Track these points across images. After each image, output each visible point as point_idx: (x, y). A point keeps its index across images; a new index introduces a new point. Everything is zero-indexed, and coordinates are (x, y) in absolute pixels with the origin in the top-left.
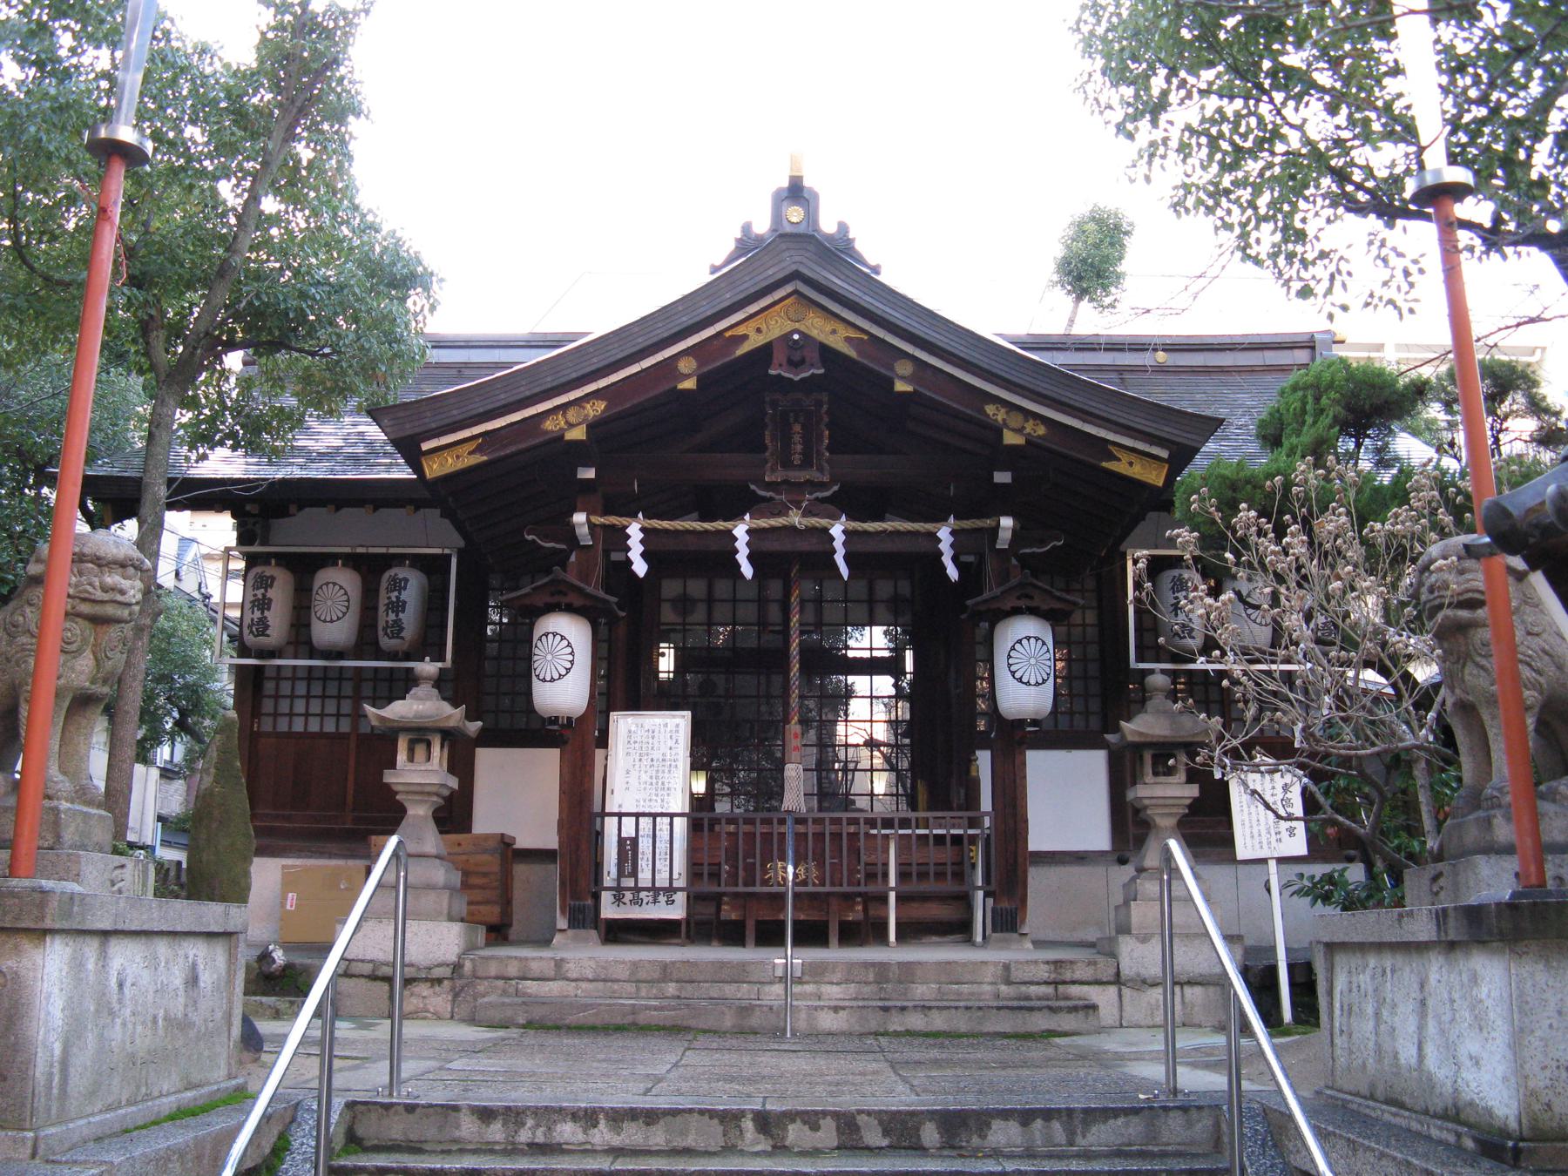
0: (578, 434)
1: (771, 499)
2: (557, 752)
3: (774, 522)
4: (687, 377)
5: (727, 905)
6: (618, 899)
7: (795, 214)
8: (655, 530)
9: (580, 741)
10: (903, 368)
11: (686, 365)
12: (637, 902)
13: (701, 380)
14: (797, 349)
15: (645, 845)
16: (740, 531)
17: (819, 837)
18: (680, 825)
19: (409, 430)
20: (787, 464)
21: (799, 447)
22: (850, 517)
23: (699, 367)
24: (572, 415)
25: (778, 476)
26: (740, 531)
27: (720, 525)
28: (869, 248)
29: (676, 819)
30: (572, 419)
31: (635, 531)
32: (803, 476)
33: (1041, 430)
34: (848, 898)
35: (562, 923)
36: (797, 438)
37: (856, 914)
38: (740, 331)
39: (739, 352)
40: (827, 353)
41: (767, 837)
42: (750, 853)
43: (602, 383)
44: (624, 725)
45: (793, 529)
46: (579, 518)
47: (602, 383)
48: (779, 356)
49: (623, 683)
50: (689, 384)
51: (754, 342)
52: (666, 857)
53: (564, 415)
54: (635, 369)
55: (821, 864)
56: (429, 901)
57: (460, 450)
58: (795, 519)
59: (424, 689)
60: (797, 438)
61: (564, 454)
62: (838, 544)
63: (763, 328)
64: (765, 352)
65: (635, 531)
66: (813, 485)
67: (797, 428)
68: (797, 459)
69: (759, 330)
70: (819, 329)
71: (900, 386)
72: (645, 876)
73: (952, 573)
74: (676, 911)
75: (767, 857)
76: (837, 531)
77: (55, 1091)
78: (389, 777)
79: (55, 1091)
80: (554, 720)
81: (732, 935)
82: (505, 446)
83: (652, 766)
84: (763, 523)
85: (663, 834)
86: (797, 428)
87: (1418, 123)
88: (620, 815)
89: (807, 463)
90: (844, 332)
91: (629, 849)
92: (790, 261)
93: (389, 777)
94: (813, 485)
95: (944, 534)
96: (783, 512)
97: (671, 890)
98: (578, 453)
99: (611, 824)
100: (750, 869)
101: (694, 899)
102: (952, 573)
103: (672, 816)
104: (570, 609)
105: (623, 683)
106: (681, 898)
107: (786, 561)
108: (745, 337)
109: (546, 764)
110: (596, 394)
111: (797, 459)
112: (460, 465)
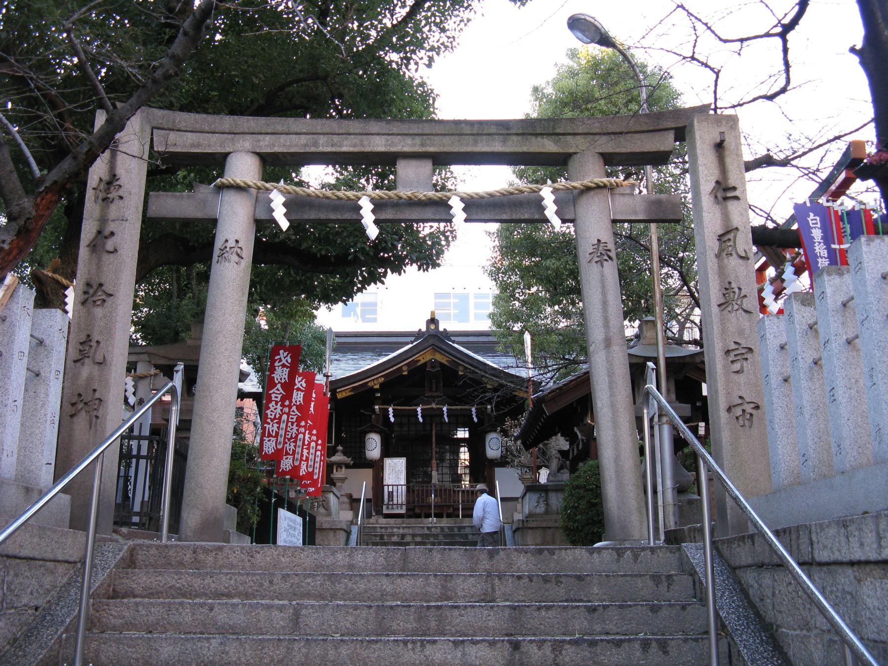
0: (377, 387)
2: (371, 470)
5: (416, 508)
6: (388, 508)
7: (433, 327)
9: (377, 467)
10: (461, 368)
11: (405, 368)
12: (393, 508)
14: (434, 363)
15: (395, 494)
16: (419, 409)
17: (441, 490)
18: (404, 488)
19: (334, 387)
20: (431, 391)
25: (429, 394)
26: (419, 409)
27: (414, 407)
31: (391, 410)
32: (436, 394)
34: (448, 507)
35: (374, 514)
37: (451, 511)
40: (441, 364)
41: (427, 491)
42: (423, 495)
44: (389, 462)
46: (377, 407)
48: (429, 365)
49: (388, 452)
50: (405, 373)
51: (422, 361)
52: (401, 496)
55: (441, 497)
56: (344, 505)
58: (434, 406)
59: (339, 453)
61: (372, 390)
62: (445, 413)
63: (425, 357)
64: (425, 364)
65: (391, 410)
66: (438, 397)
70: (439, 357)
71: (460, 373)
72: (395, 502)
73: (475, 420)
74: (403, 511)
75: (427, 496)
76: (445, 409)
77: (833, 188)
78: (332, 476)
79: (833, 188)
80: (371, 461)
81: (419, 516)
83: (395, 471)
85: (400, 491)
89: (437, 391)
90: (445, 359)
91: (391, 494)
92: (431, 341)
93: (332, 476)
94: (438, 397)
95: (473, 409)
96: (430, 404)
97: (402, 504)
98: (377, 391)
99: (386, 488)
100: (423, 499)
101: (407, 509)
102: (475, 420)
104: (376, 432)
105: (388, 452)
106: (404, 507)
107: (432, 416)
109: (368, 473)
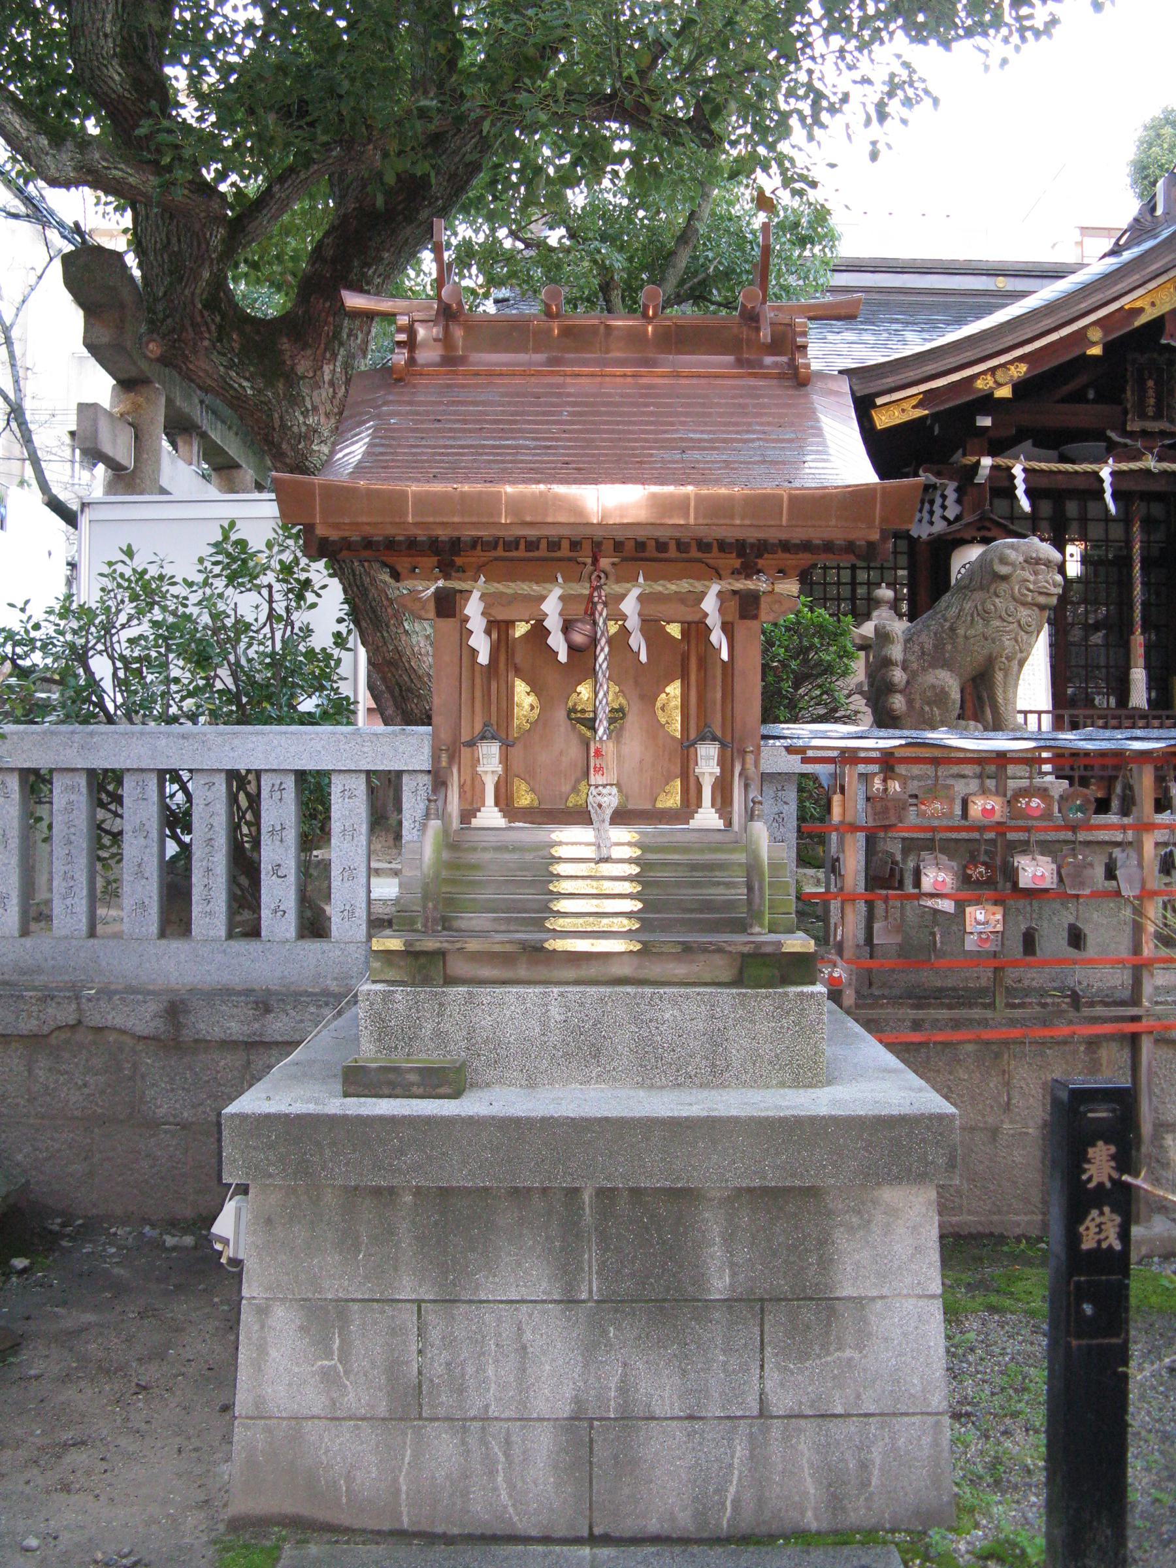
1: (1126, 445)
3: (1134, 466)
4: (1094, 344)
8: (1034, 471)
11: (1096, 335)
13: (1107, 347)
20: (1143, 416)
21: (1152, 401)
22: (1027, 459)
23: (1105, 335)
24: (1000, 376)
25: (1134, 426)
28: (64, 190)
29: (1044, 716)
30: (1001, 380)
32: (1155, 426)
33: (1023, 368)
36: (1151, 393)
38: (1138, 304)
39: (1137, 323)
43: (1028, 349)
45: (1147, 472)
47: (1028, 349)
50: (1096, 351)
53: (993, 375)
54: (1054, 337)
57: (905, 405)
60: (1151, 393)
67: (1150, 383)
68: (1150, 412)
69: (1153, 304)
76: (1105, 473)
82: (943, 402)
84: (1124, 466)
86: (1150, 383)
87: (921, 46)
88: (1025, 713)
89: (1158, 416)
103: (1039, 713)
108: (1141, 310)
110: (1020, 359)
111: (1150, 412)
112: (905, 418)
